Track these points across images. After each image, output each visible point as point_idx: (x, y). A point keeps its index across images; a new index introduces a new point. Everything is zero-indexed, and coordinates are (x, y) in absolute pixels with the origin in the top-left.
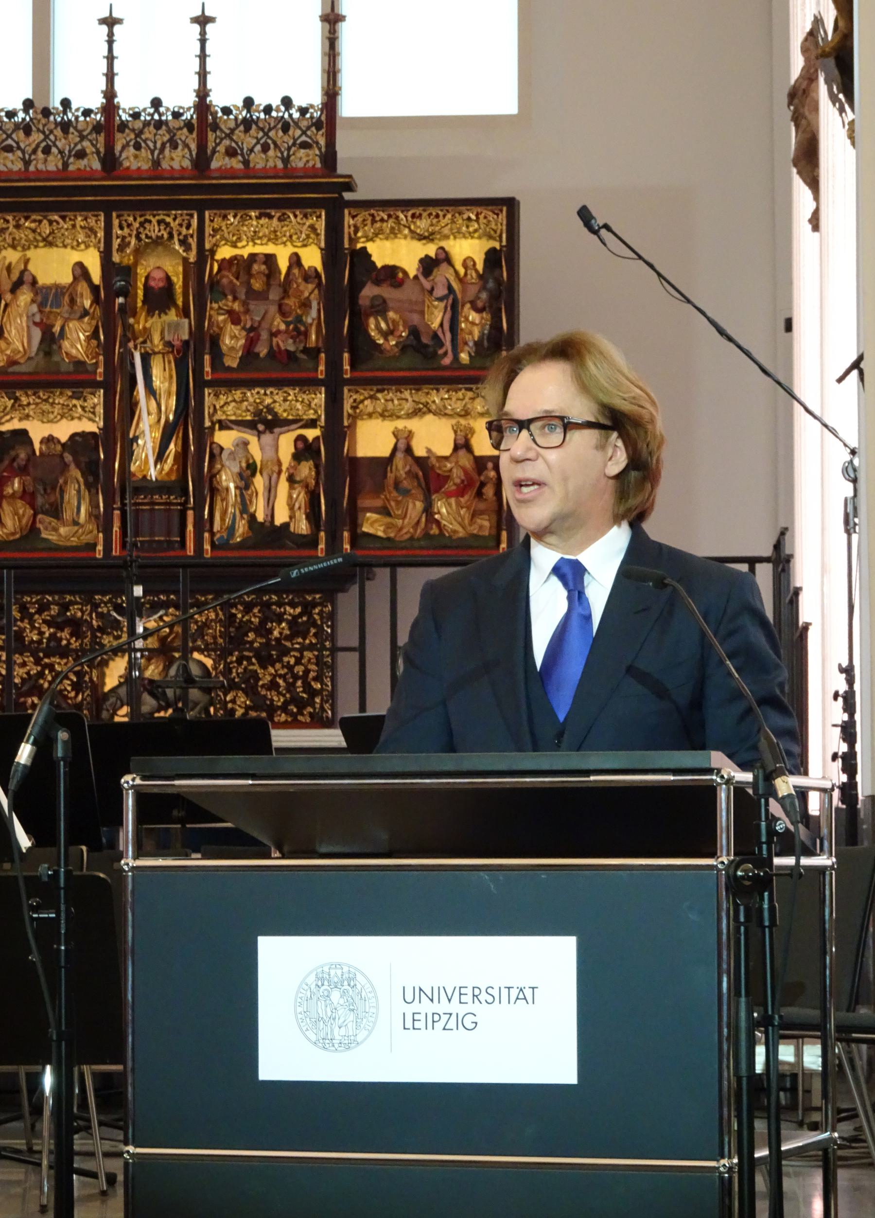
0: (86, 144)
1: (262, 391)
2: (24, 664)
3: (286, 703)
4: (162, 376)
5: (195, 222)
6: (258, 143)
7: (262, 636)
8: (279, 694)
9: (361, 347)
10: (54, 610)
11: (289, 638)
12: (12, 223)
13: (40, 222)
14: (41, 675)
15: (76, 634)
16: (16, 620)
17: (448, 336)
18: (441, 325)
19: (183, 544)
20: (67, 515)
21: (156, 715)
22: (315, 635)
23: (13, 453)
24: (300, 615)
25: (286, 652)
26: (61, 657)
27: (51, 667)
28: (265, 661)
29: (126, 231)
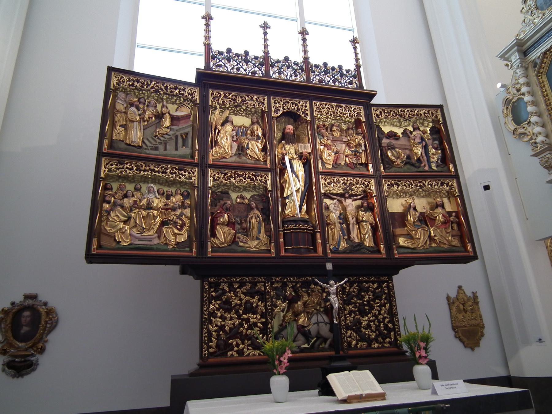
0: (256, 69)
1: (346, 179)
2: (231, 319)
3: (377, 336)
4: (299, 166)
5: (308, 105)
6: (331, 79)
7: (360, 300)
8: (372, 331)
9: (388, 163)
10: (248, 286)
11: (374, 300)
12: (222, 95)
13: (236, 97)
14: (241, 325)
15: (262, 299)
16: (227, 292)
17: (425, 158)
18: (421, 154)
19: (315, 251)
20: (255, 234)
21: (303, 346)
22: (385, 299)
23: (222, 202)
24: (377, 288)
25: (372, 308)
26: (254, 314)
27: (248, 320)
28: (363, 313)
29: (277, 105)
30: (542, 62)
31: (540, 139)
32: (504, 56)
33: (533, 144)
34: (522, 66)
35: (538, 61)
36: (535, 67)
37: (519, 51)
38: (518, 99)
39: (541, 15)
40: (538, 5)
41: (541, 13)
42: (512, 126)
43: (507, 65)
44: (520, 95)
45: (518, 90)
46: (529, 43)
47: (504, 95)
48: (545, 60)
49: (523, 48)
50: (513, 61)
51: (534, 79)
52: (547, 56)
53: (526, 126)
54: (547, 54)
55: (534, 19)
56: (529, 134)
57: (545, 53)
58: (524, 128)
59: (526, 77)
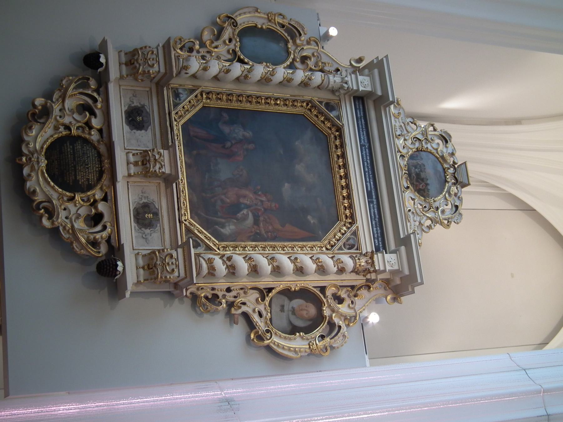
30: (327, 119)
31: (195, 65)
32: (378, 67)
33: (190, 45)
34: (342, 87)
35: (332, 115)
36: (328, 105)
37: (370, 94)
38: (289, 53)
39: (404, 151)
40: (422, 153)
41: (407, 153)
42: (244, 20)
43: (360, 60)
44: (294, 60)
45: (304, 59)
46: (372, 114)
47: (309, 32)
48: (329, 125)
49: (371, 104)
50: (360, 78)
51: (308, 95)
52: (334, 129)
53: (232, 46)
54: (337, 131)
55: (405, 140)
56: (214, 45)
57: (340, 129)
58: (230, 40)
59: (319, 87)
